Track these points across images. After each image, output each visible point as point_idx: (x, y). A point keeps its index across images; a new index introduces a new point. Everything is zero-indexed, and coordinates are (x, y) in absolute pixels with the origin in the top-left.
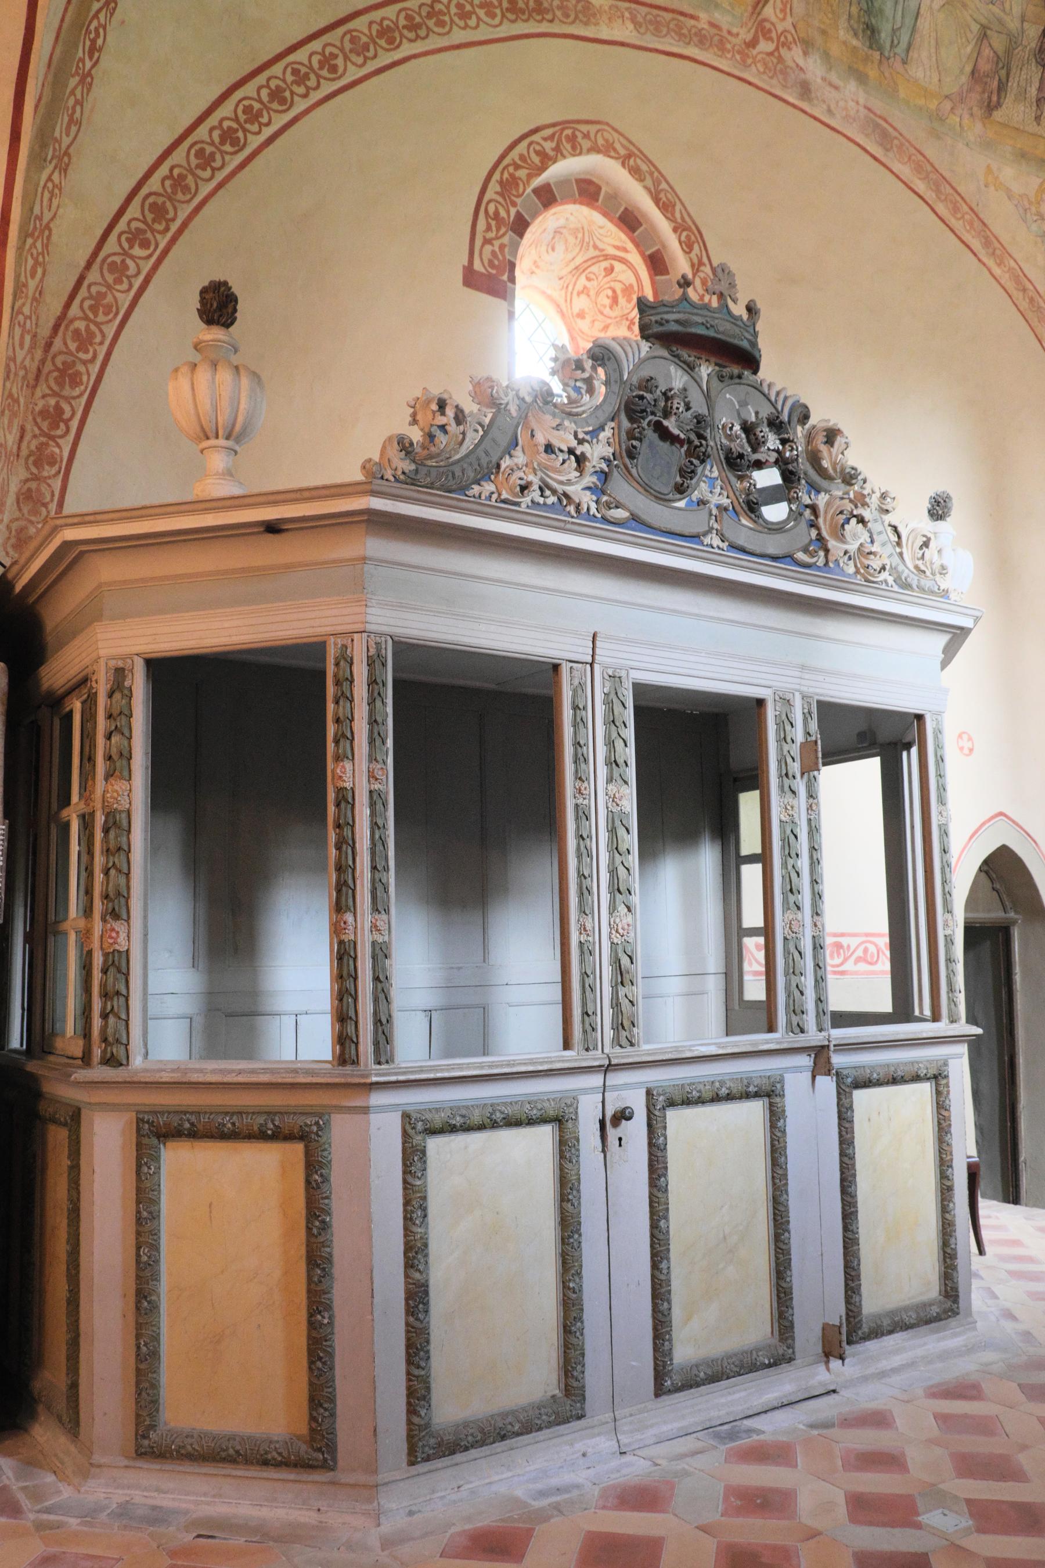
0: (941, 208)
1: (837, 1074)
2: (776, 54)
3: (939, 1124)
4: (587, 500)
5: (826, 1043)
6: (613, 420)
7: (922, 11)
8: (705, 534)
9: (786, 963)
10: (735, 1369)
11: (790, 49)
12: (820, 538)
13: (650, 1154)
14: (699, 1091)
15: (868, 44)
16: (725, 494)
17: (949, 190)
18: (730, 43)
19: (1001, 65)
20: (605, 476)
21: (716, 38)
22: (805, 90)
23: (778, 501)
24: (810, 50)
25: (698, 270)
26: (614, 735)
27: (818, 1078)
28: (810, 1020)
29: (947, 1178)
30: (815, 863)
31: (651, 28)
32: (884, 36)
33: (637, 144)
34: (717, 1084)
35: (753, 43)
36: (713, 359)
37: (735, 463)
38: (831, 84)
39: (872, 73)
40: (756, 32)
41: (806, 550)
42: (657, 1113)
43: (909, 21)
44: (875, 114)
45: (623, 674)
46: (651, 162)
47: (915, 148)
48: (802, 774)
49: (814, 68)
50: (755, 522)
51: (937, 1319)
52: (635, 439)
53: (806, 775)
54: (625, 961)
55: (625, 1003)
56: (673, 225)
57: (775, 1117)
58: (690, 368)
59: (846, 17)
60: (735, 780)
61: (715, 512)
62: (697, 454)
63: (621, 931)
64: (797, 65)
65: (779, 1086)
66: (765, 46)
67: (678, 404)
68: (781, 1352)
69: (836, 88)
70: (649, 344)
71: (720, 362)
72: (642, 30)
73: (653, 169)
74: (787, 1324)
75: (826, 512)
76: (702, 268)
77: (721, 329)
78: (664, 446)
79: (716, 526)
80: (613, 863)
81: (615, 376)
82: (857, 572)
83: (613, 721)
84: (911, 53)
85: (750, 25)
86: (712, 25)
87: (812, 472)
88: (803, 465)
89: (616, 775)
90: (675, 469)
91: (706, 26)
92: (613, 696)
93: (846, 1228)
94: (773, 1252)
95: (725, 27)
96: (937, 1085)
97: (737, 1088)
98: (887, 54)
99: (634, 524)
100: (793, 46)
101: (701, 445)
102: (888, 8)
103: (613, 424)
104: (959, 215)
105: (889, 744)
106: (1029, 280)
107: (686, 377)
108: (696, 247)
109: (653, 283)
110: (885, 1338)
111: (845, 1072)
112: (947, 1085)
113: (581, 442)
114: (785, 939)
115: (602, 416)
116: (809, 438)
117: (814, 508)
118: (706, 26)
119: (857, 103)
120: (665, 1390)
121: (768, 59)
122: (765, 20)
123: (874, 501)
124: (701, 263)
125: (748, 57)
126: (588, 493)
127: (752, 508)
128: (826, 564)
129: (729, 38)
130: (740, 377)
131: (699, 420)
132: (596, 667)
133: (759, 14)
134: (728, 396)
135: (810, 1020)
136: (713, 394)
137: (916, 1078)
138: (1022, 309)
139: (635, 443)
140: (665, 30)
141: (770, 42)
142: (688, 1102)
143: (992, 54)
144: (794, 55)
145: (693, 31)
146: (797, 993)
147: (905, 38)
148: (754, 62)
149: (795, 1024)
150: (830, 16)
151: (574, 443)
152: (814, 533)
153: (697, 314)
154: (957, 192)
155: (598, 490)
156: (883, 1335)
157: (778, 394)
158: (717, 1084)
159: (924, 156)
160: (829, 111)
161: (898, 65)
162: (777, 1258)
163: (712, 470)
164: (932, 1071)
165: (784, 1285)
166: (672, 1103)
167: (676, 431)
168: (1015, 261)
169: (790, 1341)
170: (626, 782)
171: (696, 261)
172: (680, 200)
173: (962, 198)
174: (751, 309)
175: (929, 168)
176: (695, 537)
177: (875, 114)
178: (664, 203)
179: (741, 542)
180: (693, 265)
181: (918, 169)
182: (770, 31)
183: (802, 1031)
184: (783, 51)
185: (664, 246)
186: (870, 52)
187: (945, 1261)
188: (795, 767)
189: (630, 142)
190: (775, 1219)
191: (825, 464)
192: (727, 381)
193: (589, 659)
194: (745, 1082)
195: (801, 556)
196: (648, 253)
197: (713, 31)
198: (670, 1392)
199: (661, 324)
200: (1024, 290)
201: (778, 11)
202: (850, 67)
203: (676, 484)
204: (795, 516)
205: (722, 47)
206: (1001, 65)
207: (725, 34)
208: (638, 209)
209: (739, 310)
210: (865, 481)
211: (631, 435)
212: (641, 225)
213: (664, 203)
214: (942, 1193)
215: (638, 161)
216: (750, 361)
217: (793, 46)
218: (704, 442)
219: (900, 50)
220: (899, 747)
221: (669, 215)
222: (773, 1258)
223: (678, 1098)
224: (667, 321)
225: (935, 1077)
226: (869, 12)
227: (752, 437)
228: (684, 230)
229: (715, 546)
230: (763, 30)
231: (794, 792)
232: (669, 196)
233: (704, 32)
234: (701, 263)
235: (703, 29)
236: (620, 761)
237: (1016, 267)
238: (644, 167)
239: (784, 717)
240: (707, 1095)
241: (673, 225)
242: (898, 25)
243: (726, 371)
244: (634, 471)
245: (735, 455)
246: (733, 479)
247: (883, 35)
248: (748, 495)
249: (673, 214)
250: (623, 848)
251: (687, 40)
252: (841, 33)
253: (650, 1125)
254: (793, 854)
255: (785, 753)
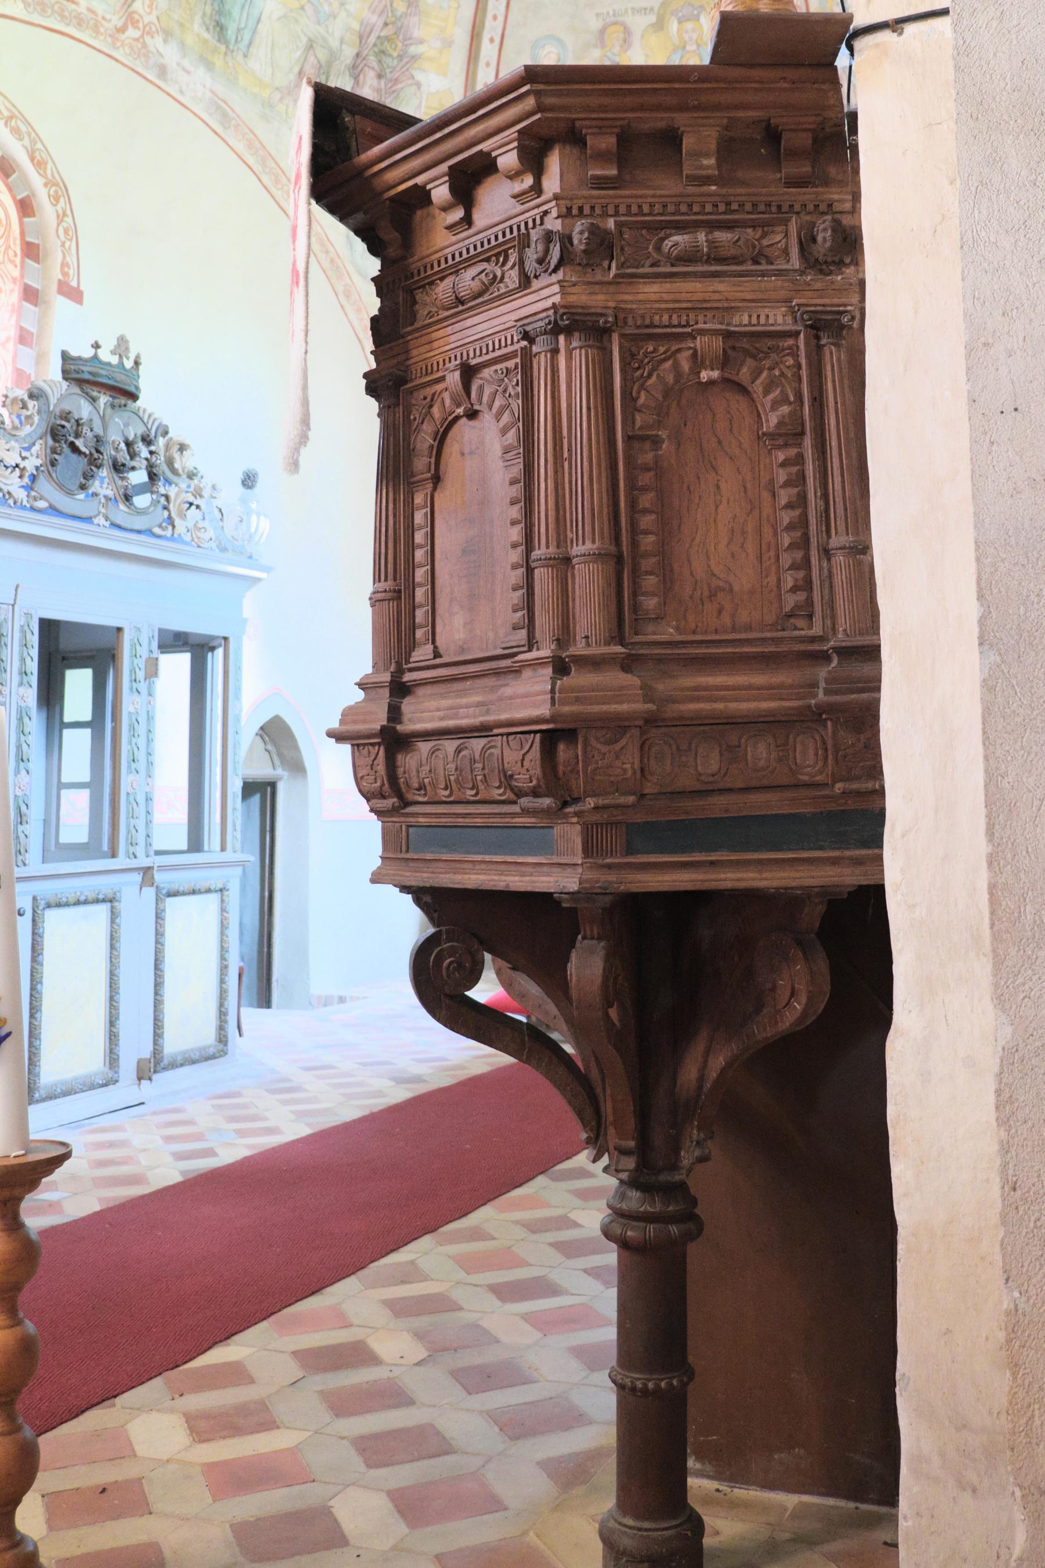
0: (265, 179)
1: (157, 887)
2: (141, 40)
3: (222, 922)
4: (21, 495)
5: (152, 865)
6: (41, 438)
7: (263, 18)
8: (95, 516)
9: (128, 811)
10: (80, 1087)
11: (153, 37)
12: (170, 517)
13: (33, 939)
14: (67, 898)
15: (217, 38)
16: (110, 487)
17: (273, 165)
18: (103, 27)
19: (322, 71)
20: (33, 478)
21: (92, 22)
22: (162, 71)
23: (144, 492)
24: (170, 38)
25: (62, 221)
26: (25, 654)
27: (144, 889)
28: (140, 850)
29: (225, 960)
30: (149, 741)
31: (39, 8)
32: (231, 33)
33: (18, 107)
34: (78, 894)
35: (122, 30)
36: (108, 393)
37: (118, 468)
38: (184, 69)
39: (219, 62)
40: (127, 20)
41: (160, 526)
42: (39, 912)
43: (251, 24)
44: (218, 98)
45: (33, 613)
46: (29, 124)
47: (248, 128)
48: (145, 679)
49: (170, 54)
50: (129, 508)
51: (213, 1057)
52: (57, 453)
53: (147, 681)
54: (23, 808)
55: (22, 836)
56: (44, 181)
57: (114, 915)
58: (94, 400)
59: (201, 14)
60: (64, 659)
61: (103, 500)
62: (94, 462)
63: (22, 788)
64: (158, 51)
65: (118, 894)
66: (132, 33)
67: (85, 429)
68: (110, 1076)
69: (188, 72)
70: (68, 383)
71: (114, 395)
72: (31, 10)
73: (30, 130)
74: (115, 1057)
75: (175, 500)
76: (65, 219)
77: (118, 379)
78: (74, 457)
79: (103, 510)
80: (19, 741)
81: (44, 408)
82: (193, 540)
83: (26, 645)
84: (251, 50)
85: (121, 14)
86: (89, 10)
87: (168, 473)
88: (163, 468)
89: (25, 681)
90: (80, 473)
91: (84, 11)
92: (26, 628)
93: (156, 993)
94: (108, 1009)
95: (100, 13)
96: (222, 895)
97: (91, 896)
98: (231, 47)
99: (50, 511)
100: (156, 35)
101: (99, 458)
102: (236, 12)
103: (41, 441)
104: (279, 186)
105: (198, 645)
106: (332, 244)
107: (91, 408)
108: (62, 200)
109: (21, 224)
110: (177, 1070)
111: (162, 886)
112: (228, 896)
113: (24, 458)
114: (128, 793)
115: (35, 437)
116: (168, 447)
117: (167, 498)
118: (84, 11)
119: (204, 87)
120: (34, 1100)
121: (134, 43)
122: (134, 12)
123: (206, 493)
124: (65, 214)
125: (118, 40)
126: (22, 490)
127: (127, 498)
128: (173, 535)
129: (104, 23)
130: (125, 405)
131: (98, 439)
132: (16, 606)
133: (129, 6)
134: (117, 420)
135: (140, 850)
136: (107, 418)
137: (209, 891)
138: (324, 267)
139: (57, 457)
140: (49, 11)
141: (137, 30)
142: (59, 905)
143: (316, 62)
144: (156, 43)
145: (73, 14)
146: (134, 831)
147: (247, 36)
148: (123, 45)
149: (131, 852)
150: (188, 12)
151: (19, 461)
152: (166, 513)
153: (102, 369)
154: (278, 165)
155: (29, 488)
156: (177, 1067)
157: (150, 416)
158: (78, 894)
159: (255, 135)
160: (181, 92)
161: (240, 57)
162: (110, 1012)
163: (104, 472)
164: (219, 886)
165: (115, 1030)
166: (49, 906)
167: (83, 449)
168: (322, 228)
169: (116, 1069)
170: (31, 686)
171: (61, 212)
172: (52, 160)
173: (283, 172)
174: (137, 363)
175: (259, 145)
176: (88, 520)
177: (218, 98)
178: (38, 161)
179: (119, 522)
180: (58, 216)
181: (250, 146)
182: (138, 21)
183: (135, 857)
184: (147, 39)
185: (34, 194)
186: (218, 45)
187: (220, 1018)
188: (140, 675)
189: (14, 106)
190: (111, 987)
191: (177, 465)
192: (117, 408)
193: (12, 602)
194: (97, 892)
195: (157, 530)
196: (19, 197)
197: (90, 15)
198: (38, 1101)
199: (78, 373)
200: (327, 252)
201: (146, 7)
202: (201, 56)
203: (81, 483)
204: (155, 503)
205: (96, 29)
206: (322, 71)
207: (100, 19)
208: (14, 160)
209: (129, 364)
210: (202, 477)
211: (54, 451)
212: (14, 172)
213: (38, 161)
214: (221, 970)
215: (19, 122)
216: (133, 397)
217: (156, 35)
218: (101, 456)
219: (243, 45)
220: (206, 648)
221: (42, 172)
222: (108, 1013)
223: (53, 903)
224: (83, 372)
225: (221, 890)
226: (220, 12)
227: (131, 450)
228: (53, 185)
229: (101, 524)
230: (131, 20)
231: (139, 692)
232: (43, 156)
233: (82, 16)
234: (65, 214)
235: (81, 13)
236: (28, 672)
237: (322, 232)
238: (23, 128)
239: (136, 640)
240: (72, 900)
241: (44, 181)
242: (242, 25)
243: (117, 401)
244: (54, 475)
245: (120, 464)
246: (116, 478)
247: (230, 32)
248: (125, 490)
249: (45, 171)
250: (26, 731)
251: (68, 21)
252: (196, 26)
253: (34, 920)
254: (136, 735)
255: (135, 665)
